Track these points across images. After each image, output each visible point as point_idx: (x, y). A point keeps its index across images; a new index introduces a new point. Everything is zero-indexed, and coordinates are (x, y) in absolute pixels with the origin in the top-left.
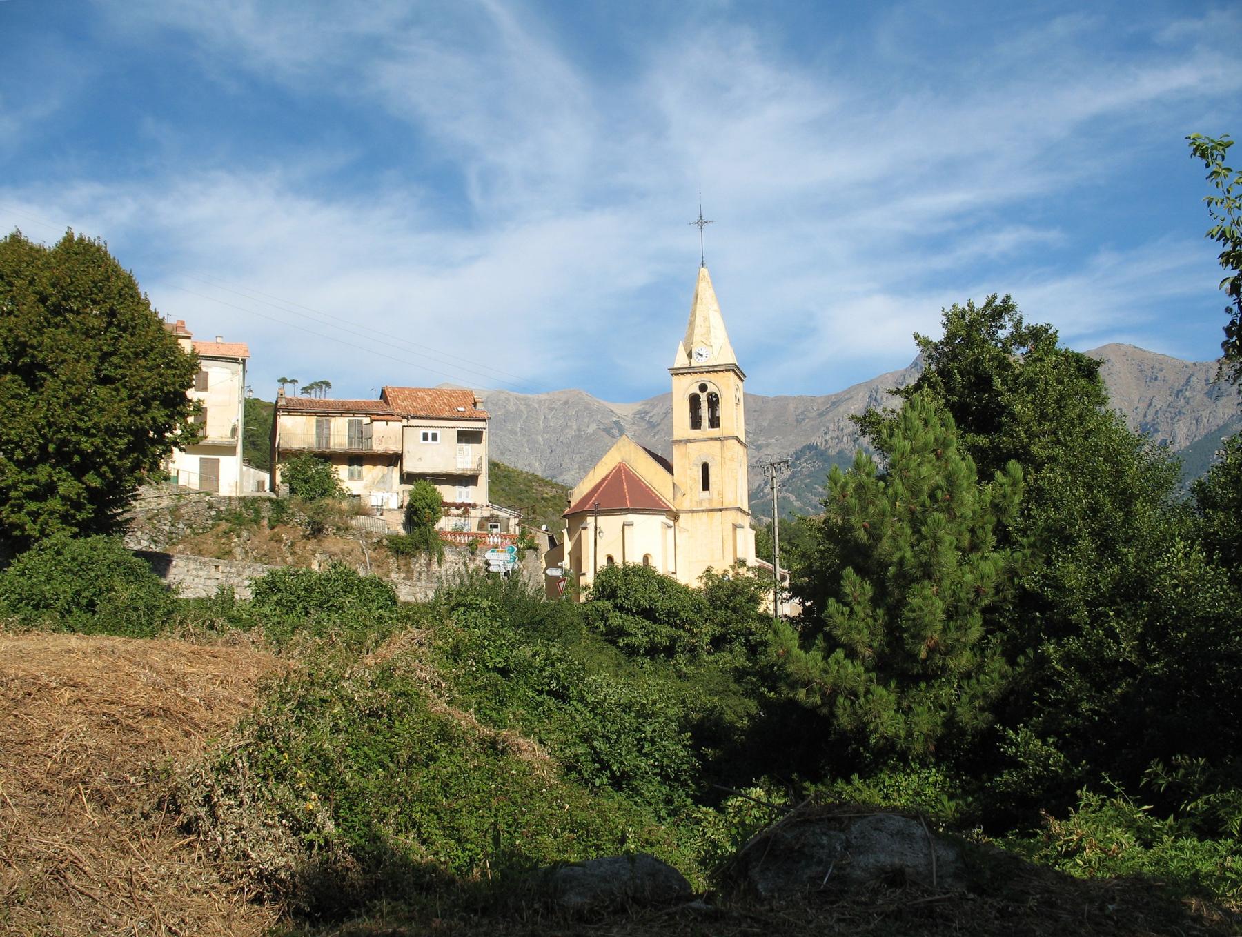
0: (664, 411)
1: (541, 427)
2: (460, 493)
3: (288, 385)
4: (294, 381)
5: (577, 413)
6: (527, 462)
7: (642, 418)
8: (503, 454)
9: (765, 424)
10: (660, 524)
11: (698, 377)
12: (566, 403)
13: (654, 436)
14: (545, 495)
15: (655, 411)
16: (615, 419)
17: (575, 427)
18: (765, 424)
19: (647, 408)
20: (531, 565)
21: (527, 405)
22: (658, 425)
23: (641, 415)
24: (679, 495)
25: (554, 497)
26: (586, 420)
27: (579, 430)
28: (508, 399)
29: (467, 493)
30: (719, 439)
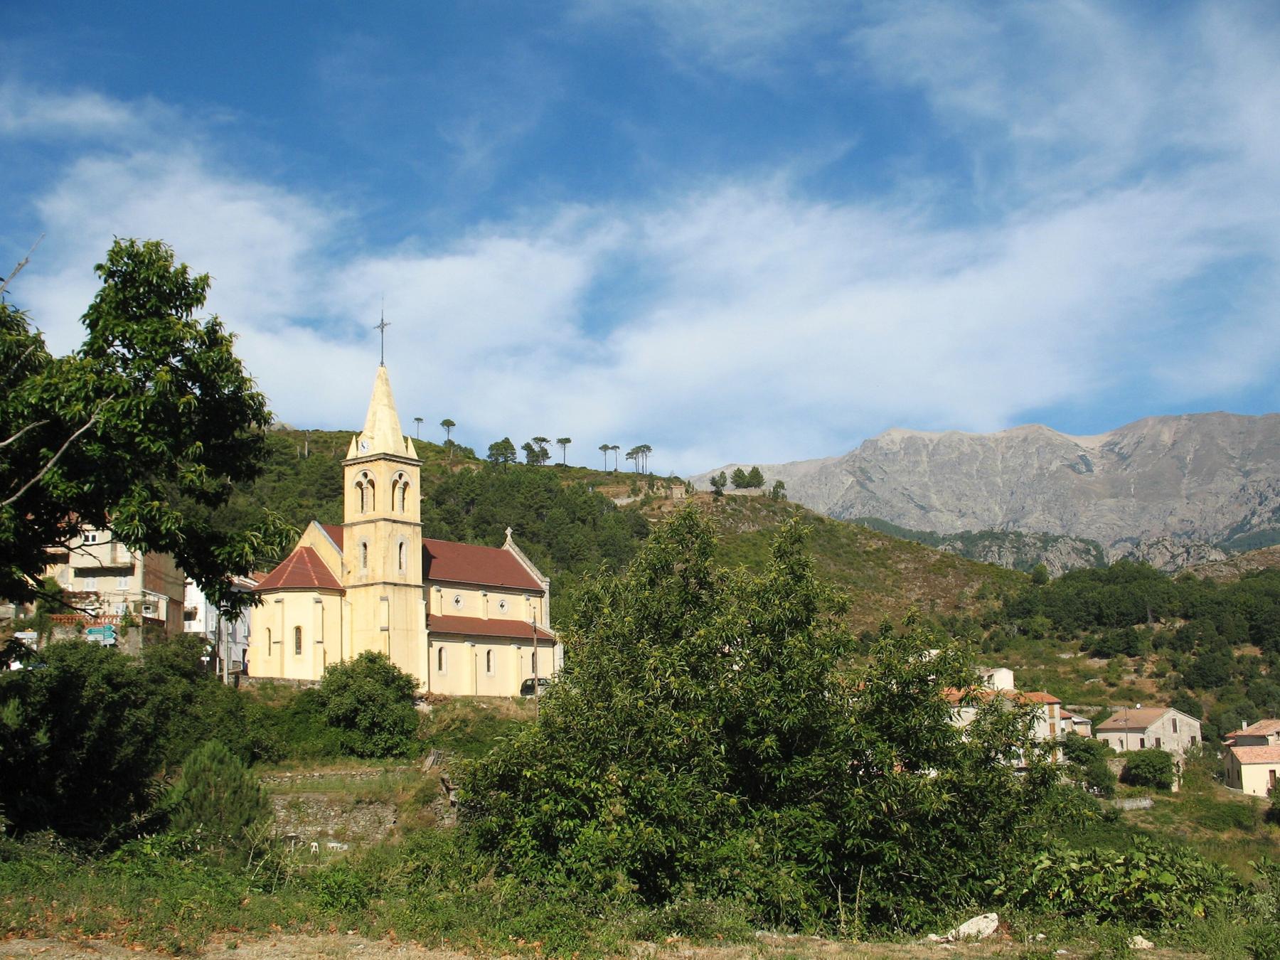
0: (1135, 440)
1: (1000, 467)
2: (120, 582)
3: (610, 452)
4: (615, 448)
5: (1037, 450)
6: (986, 507)
7: (1112, 450)
8: (959, 500)
9: (1253, 446)
10: (312, 601)
11: (361, 467)
12: (1025, 440)
13: (1125, 469)
14: (868, 549)
15: (1125, 442)
16: (1081, 453)
17: (1036, 465)
18: (1253, 446)
19: (1117, 439)
20: (132, 640)
21: (983, 445)
22: (1130, 456)
23: (1110, 447)
24: (345, 573)
25: (878, 550)
26: (1048, 456)
27: (1041, 468)
28: (961, 440)
29: (126, 582)
30: (372, 521)
